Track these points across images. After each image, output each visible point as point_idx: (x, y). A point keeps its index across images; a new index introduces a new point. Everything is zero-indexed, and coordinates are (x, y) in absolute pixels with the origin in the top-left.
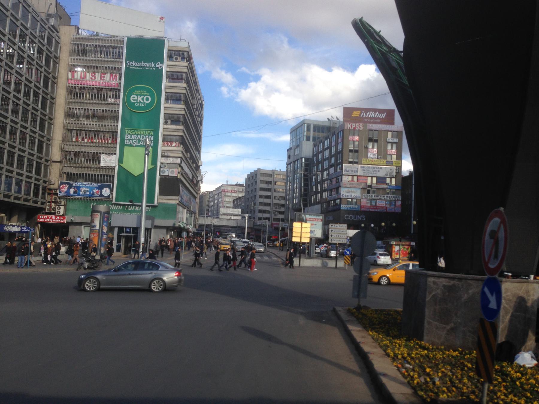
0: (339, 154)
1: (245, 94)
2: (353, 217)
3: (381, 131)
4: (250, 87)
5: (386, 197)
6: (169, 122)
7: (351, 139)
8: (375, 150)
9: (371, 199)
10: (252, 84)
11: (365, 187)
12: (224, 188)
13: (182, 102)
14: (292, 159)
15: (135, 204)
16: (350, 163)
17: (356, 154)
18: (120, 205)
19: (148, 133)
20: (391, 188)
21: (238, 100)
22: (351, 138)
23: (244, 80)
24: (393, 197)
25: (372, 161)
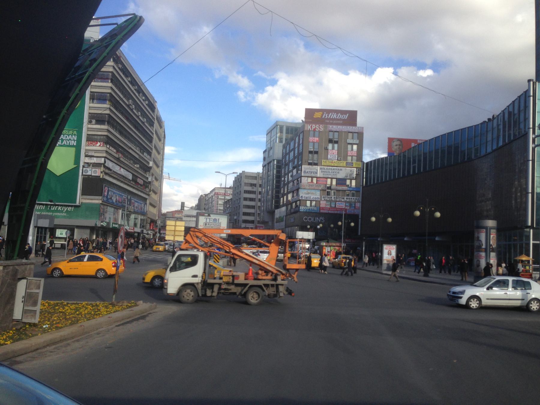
0: (300, 154)
1: (262, 98)
2: (312, 219)
3: (342, 132)
4: (267, 91)
5: (345, 199)
6: (94, 121)
7: (311, 141)
8: (335, 152)
9: (331, 201)
10: (269, 89)
11: (324, 188)
12: (216, 191)
13: (108, 102)
14: (266, 162)
15: (57, 203)
16: (310, 164)
17: (316, 155)
18: (43, 205)
19: (71, 132)
20: (351, 189)
21: (255, 104)
22: (311, 139)
23: (260, 85)
24: (353, 199)
25: (332, 162)
